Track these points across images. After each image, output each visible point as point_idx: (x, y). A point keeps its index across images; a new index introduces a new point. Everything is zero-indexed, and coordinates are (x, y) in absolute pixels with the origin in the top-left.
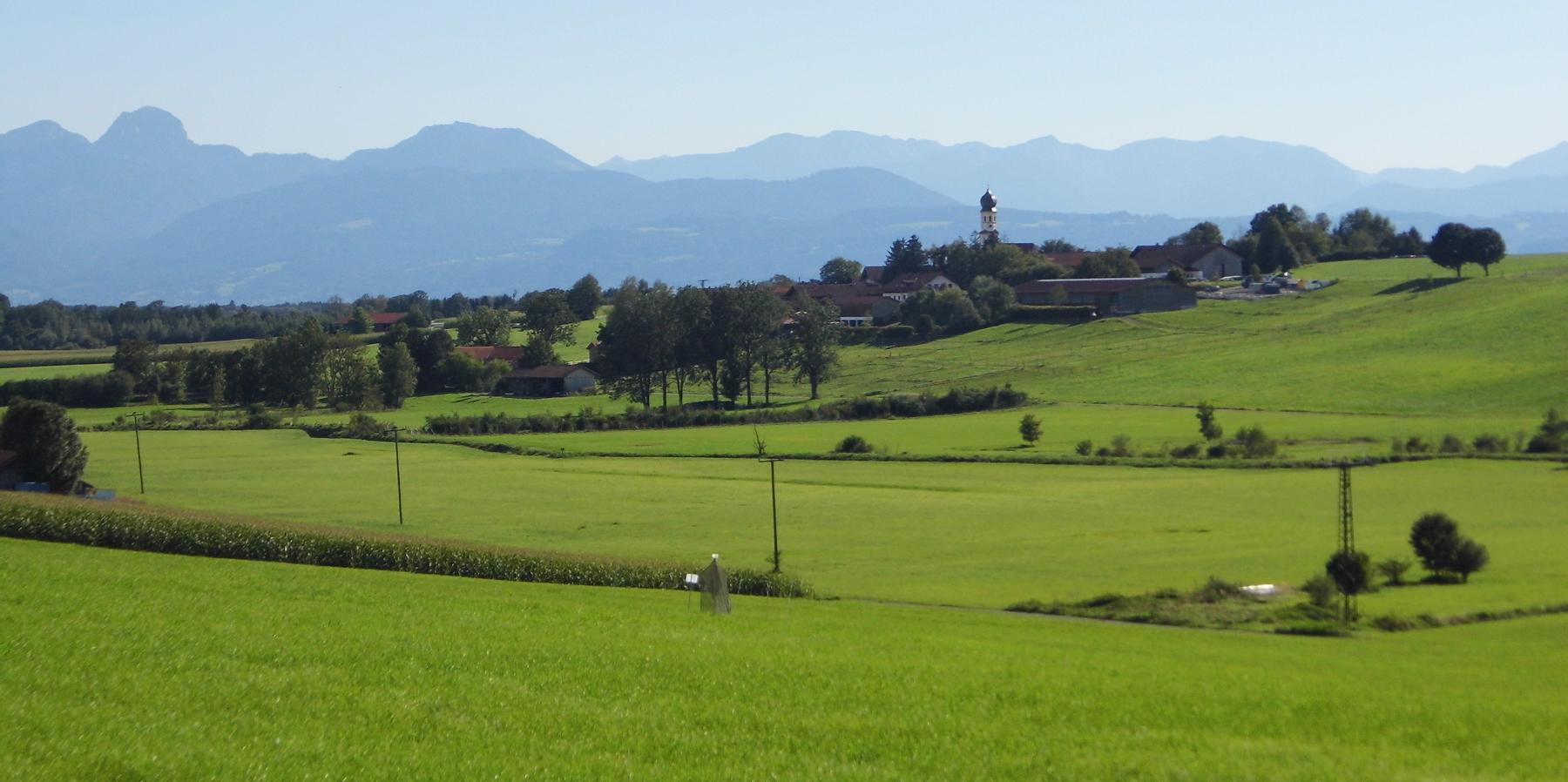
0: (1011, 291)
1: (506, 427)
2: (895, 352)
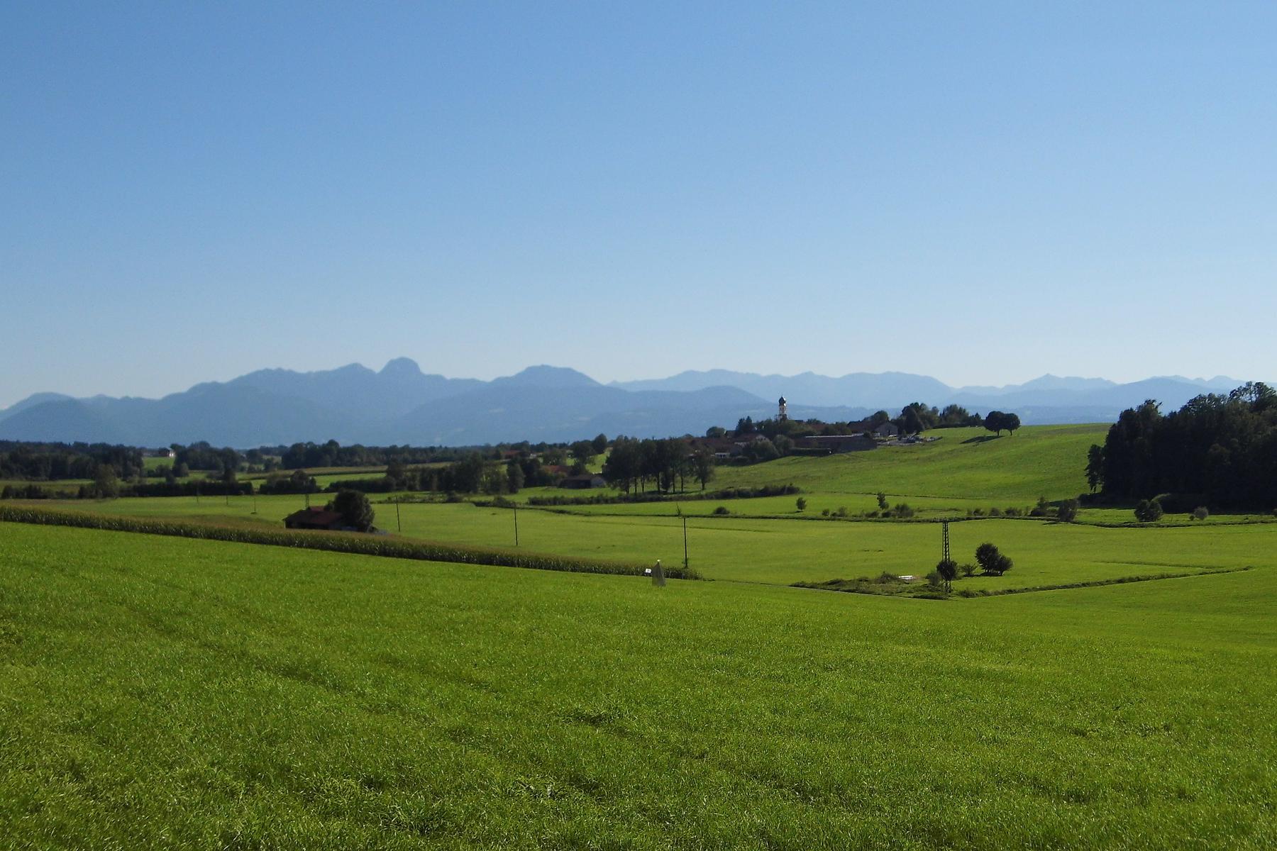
0: (792, 441)
1: (564, 502)
2: (740, 469)
